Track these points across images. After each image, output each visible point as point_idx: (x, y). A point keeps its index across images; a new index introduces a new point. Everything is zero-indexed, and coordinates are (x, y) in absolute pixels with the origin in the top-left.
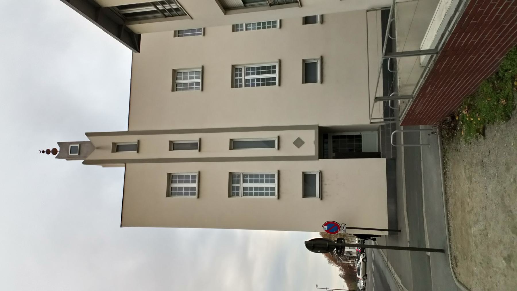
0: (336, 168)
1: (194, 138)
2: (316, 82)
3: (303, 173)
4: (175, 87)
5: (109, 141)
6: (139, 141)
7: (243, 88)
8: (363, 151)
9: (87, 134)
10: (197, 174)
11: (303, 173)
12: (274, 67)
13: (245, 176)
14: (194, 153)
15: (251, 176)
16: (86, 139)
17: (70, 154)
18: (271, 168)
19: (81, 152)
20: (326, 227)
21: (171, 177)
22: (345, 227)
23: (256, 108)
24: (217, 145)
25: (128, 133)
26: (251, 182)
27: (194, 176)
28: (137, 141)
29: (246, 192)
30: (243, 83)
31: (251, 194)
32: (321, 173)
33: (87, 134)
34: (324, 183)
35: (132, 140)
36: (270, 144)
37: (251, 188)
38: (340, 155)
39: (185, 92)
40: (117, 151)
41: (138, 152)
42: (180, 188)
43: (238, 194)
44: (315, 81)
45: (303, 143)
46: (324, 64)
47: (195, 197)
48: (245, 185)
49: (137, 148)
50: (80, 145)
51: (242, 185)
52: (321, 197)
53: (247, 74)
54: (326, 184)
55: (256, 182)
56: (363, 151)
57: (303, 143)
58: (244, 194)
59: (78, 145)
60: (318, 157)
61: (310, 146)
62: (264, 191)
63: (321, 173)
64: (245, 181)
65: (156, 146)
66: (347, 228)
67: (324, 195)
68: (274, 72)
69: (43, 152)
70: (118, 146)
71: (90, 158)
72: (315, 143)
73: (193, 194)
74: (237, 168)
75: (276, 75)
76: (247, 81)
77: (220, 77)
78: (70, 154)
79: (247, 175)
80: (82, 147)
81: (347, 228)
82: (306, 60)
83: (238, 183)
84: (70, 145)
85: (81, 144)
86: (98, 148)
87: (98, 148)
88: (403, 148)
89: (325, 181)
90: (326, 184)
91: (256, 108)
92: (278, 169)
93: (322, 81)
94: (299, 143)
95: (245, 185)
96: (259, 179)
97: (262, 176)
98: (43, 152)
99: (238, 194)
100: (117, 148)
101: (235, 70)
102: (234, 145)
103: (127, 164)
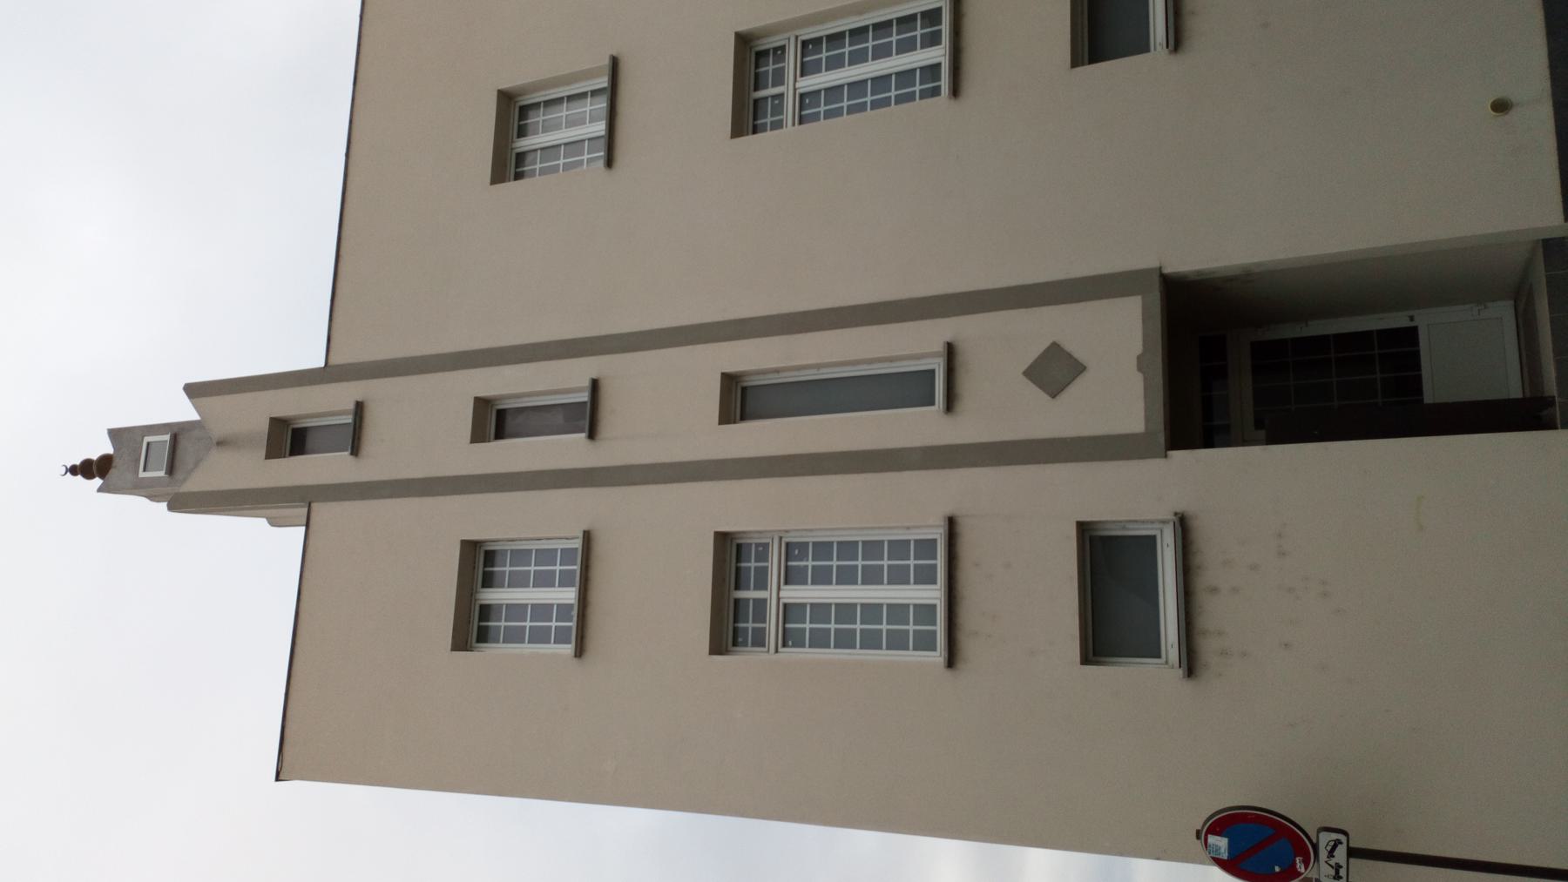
0: (1271, 501)
1: (914, 346)
3: (1083, 528)
5: (255, 415)
6: (359, 408)
7: (790, 129)
8: (1429, 397)
10: (939, 534)
11: (1083, 528)
13: (792, 550)
14: (568, 449)
15: (822, 549)
16: (185, 412)
17: (142, 474)
18: (911, 507)
19: (177, 464)
20: (1221, 843)
21: (732, 556)
22: (1341, 853)
24: (665, 406)
25: (328, 374)
26: (822, 577)
27: (926, 547)
28: (587, 383)
29: (795, 628)
30: (790, 104)
31: (820, 640)
32: (1183, 525)
34: (1203, 581)
35: (333, 402)
36: (906, 389)
37: (820, 611)
38: (1286, 424)
39: (551, 177)
40: (499, 435)
41: (592, 435)
42: (517, 611)
43: (759, 640)
44: (1140, 45)
45: (1077, 368)
47: (938, 656)
48: (793, 594)
49: (587, 416)
50: (175, 440)
51: (778, 594)
52: (1190, 664)
54: (1214, 590)
55: (872, 577)
56: (1429, 397)
57: (1077, 368)
58: (788, 639)
59: (167, 437)
60: (1161, 439)
61: (1118, 356)
62: (884, 627)
63: (1183, 525)
64: (790, 577)
65: (423, 427)
66: (1353, 853)
67: (1208, 648)
70: (501, 414)
71: (196, 482)
73: (925, 642)
74: (750, 508)
76: (805, 99)
78: (142, 474)
79: (803, 546)
80: (184, 443)
81: (1353, 853)
82: (523, 90)
83: (762, 584)
84: (147, 439)
85: (177, 433)
86: (220, 443)
87: (220, 443)
89: (1210, 574)
90: (1214, 590)
92: (950, 510)
93: (1176, 41)
94: (1055, 371)
95: (793, 594)
96: (860, 563)
97: (872, 549)
99: (759, 640)
100: (291, 438)
101: (753, 57)
102: (740, 399)
103: (314, 506)
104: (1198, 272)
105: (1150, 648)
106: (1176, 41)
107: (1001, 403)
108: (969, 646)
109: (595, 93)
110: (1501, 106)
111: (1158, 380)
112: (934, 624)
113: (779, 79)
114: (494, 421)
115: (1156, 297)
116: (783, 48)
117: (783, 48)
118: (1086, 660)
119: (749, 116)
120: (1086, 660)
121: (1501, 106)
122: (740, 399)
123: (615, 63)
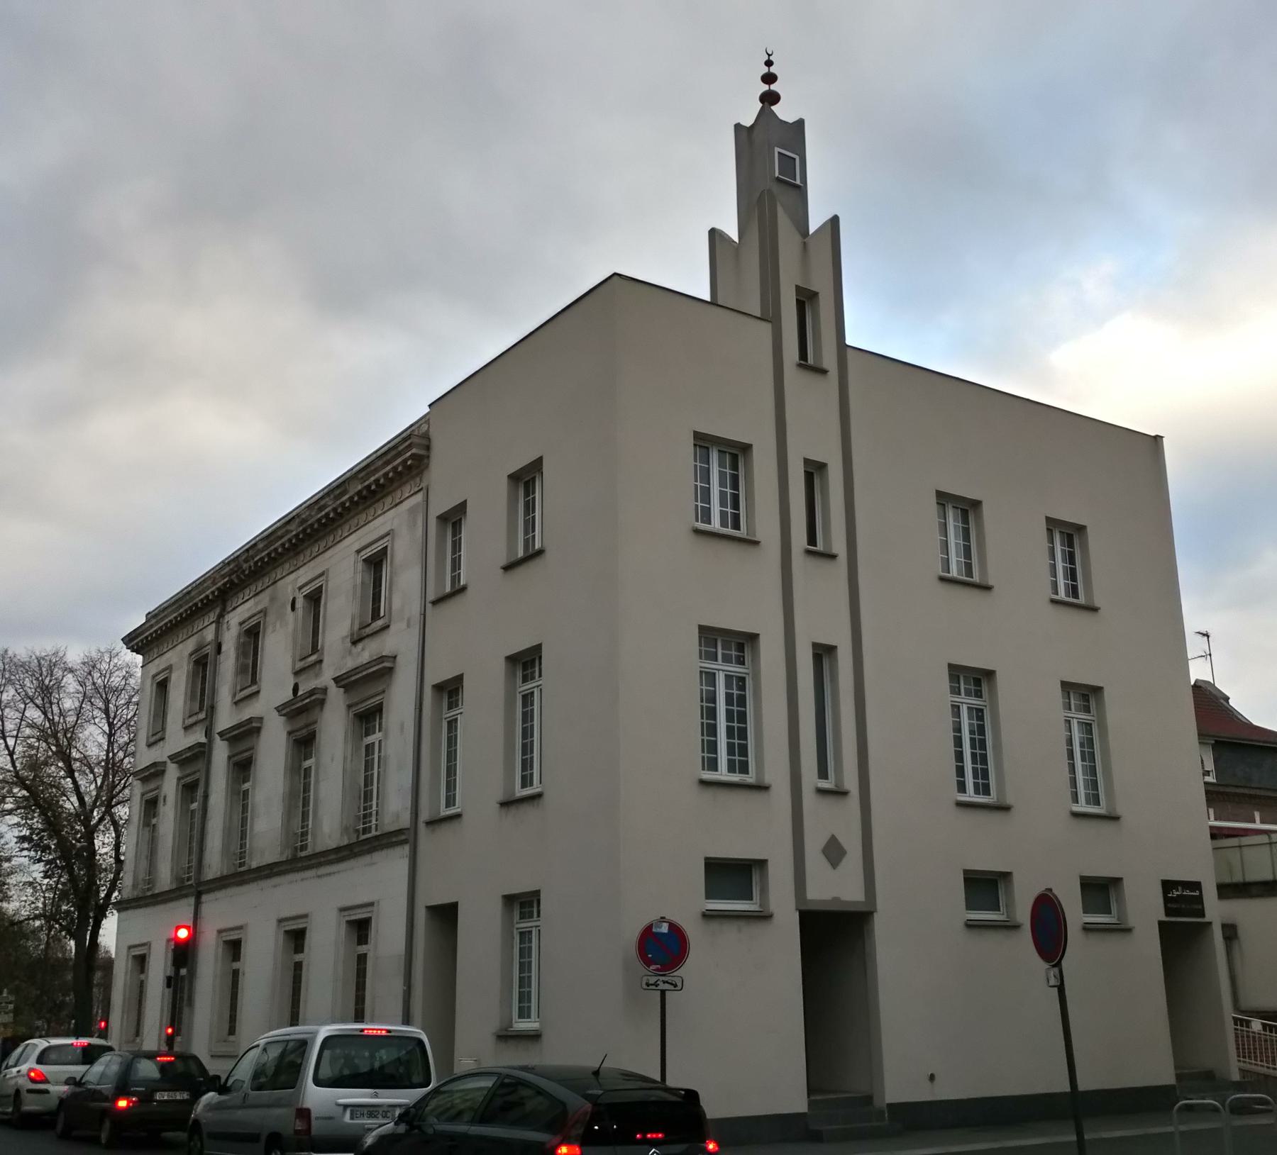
2: (707, 898)
4: (703, 442)
5: (820, 284)
9: (835, 221)
12: (744, 769)
17: (777, 150)
18: (775, 770)
20: (664, 929)
21: (736, 453)
23: (908, 731)
25: (842, 348)
33: (835, 221)
44: (970, 906)
46: (742, 923)
50: (797, 187)
53: (728, 678)
59: (798, 182)
61: (835, 887)
66: (663, 992)
67: (715, 925)
68: (731, 768)
69: (769, 63)
72: (836, 900)
75: (723, 774)
77: (974, 632)
81: (663, 992)
82: (979, 518)
88: (1170, 1129)
91: (908, 731)
98: (769, 63)
104: (873, 930)
105: (710, 895)
106: (970, 925)
107: (827, 819)
108: (709, 793)
109: (969, 567)
110: (932, 1077)
111: (852, 909)
112: (1262, 822)
113: (727, 659)
114: (814, 471)
115: (864, 909)
116: (981, 697)
117: (981, 697)
118: (966, 872)
119: (709, 636)
120: (966, 872)
121: (932, 1077)
122: (823, 653)
123: (1094, 610)
